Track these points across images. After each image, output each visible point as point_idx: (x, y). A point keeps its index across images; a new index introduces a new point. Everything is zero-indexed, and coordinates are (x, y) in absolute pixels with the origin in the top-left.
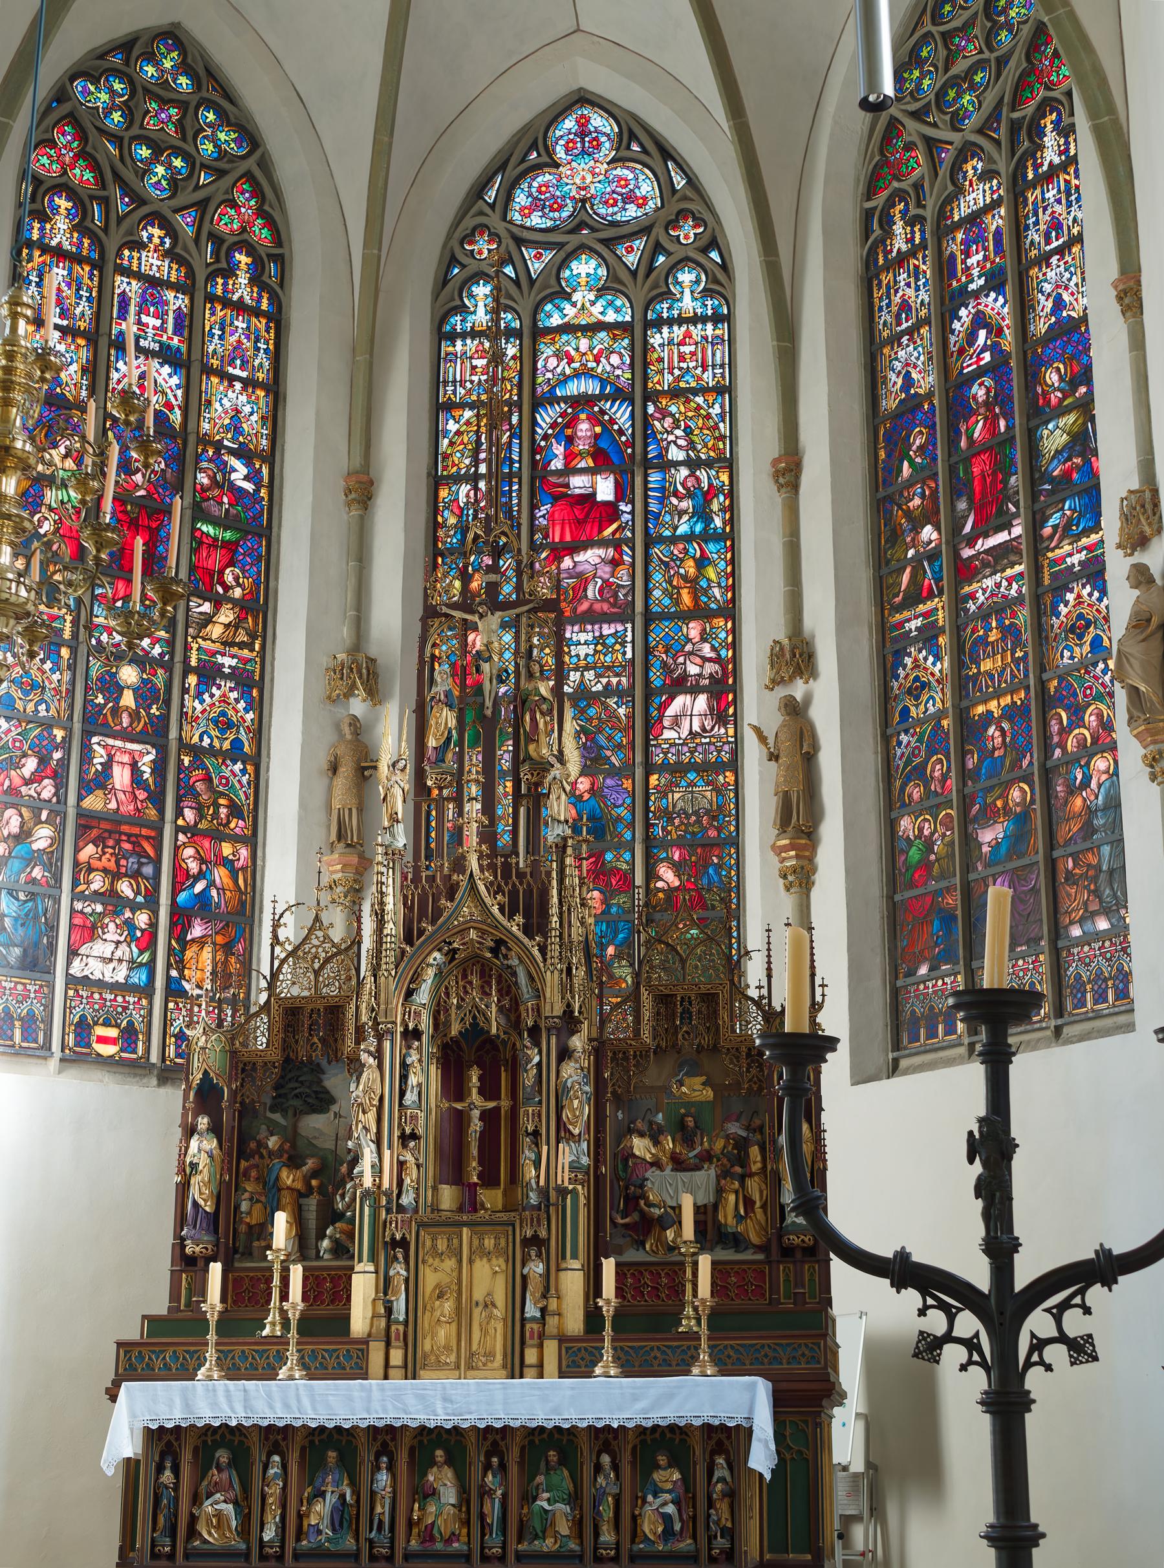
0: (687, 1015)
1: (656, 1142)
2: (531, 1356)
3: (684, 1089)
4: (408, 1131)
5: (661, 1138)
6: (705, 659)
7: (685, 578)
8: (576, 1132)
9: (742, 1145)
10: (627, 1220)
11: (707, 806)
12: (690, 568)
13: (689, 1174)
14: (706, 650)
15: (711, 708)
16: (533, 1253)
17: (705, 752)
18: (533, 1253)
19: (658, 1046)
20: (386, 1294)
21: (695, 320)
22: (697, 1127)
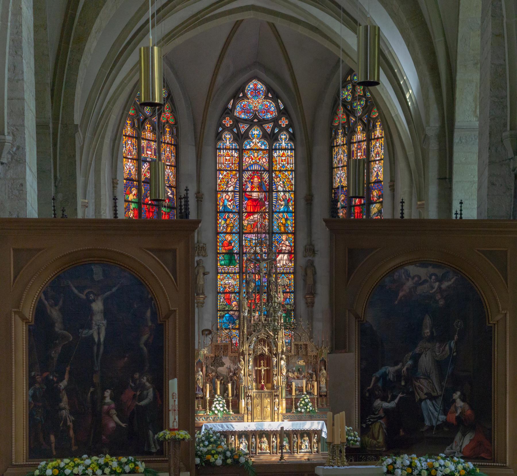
1: (294, 374)
2: (276, 417)
6: (287, 246)
7: (282, 223)
9: (311, 375)
12: (283, 221)
14: (287, 243)
15: (288, 258)
21: (285, 149)
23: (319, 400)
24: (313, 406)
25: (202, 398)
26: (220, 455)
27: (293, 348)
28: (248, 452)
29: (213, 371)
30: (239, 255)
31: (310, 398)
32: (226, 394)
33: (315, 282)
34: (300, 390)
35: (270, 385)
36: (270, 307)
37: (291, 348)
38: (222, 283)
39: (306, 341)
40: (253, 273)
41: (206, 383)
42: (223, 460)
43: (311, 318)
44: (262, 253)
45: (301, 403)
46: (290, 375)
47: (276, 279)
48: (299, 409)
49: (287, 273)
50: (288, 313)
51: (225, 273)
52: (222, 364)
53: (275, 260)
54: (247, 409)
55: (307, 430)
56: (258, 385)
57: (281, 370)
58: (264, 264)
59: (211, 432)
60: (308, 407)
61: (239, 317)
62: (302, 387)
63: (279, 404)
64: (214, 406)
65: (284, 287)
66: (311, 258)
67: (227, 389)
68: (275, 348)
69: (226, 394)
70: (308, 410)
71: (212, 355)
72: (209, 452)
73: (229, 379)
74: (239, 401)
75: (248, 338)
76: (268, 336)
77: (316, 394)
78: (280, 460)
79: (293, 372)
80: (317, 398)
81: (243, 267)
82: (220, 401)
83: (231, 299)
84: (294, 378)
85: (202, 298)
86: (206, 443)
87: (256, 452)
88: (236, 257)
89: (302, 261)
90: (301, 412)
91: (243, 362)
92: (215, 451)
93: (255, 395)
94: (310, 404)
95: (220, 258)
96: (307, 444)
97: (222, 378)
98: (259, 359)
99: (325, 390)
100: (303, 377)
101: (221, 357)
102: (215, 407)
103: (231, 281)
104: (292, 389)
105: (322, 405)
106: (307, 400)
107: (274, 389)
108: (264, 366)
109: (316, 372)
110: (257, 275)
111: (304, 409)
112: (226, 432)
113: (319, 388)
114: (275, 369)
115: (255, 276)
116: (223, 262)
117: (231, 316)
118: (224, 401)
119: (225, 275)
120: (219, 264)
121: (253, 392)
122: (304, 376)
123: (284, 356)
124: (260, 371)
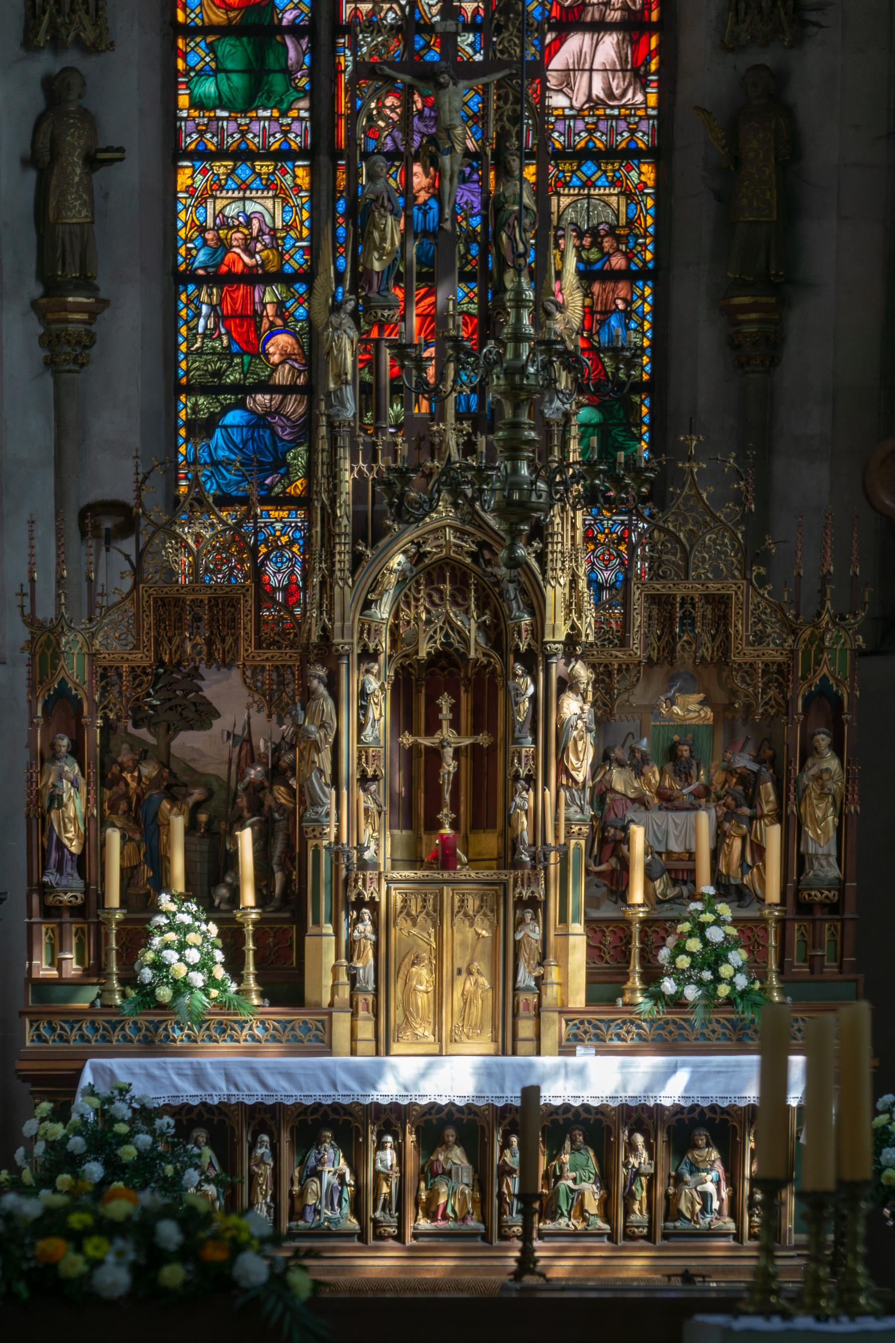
0: (688, 620)
1: (639, 774)
2: (526, 1028)
3: (676, 709)
4: (370, 772)
5: (646, 769)
8: (580, 778)
9: (749, 785)
10: (603, 867)
11: (611, 218)
13: (683, 814)
15: (623, 59)
16: (528, 916)
17: (612, 132)
18: (528, 916)
19: (649, 658)
20: (350, 958)
22: (692, 757)
23: (795, 932)
24: (755, 967)
25: (78, 911)
26: (119, 1243)
27: (638, 620)
28: (353, 1224)
29: (144, 756)
30: (314, 41)
31: (736, 922)
32: (224, 892)
33: (790, 208)
34: (674, 870)
35: (489, 842)
36: (489, 366)
37: (626, 618)
38: (208, 214)
39: (718, 575)
40: (393, 156)
41: (104, 823)
42: (135, 1270)
43: (757, 434)
44: (451, 26)
45: (680, 949)
46: (619, 780)
47: (542, 191)
48: (669, 986)
49: (611, 154)
50: (612, 399)
51: (221, 154)
52: (203, 715)
53: (539, 69)
54: (353, 979)
55: (713, 1108)
56: (417, 840)
57: (562, 750)
58: (463, 98)
59: (122, 1109)
60: (726, 971)
61: (306, 430)
62: (691, 856)
63: (544, 956)
64: (150, 956)
65: (597, 243)
66: (766, 57)
67: (232, 860)
68: (526, 620)
69: (224, 892)
70: (723, 990)
71: (143, 658)
72: (52, 1222)
73: (242, 801)
74: (302, 931)
75: (357, 560)
76: (482, 545)
77: (773, 894)
78: (518, 1275)
79: (638, 767)
80: (782, 922)
81: (333, 114)
82: (188, 929)
83: (256, 317)
84: (641, 801)
85: (79, 308)
86: (95, 1170)
87: (401, 1225)
88: (294, 51)
89: (710, 76)
90: (677, 1002)
91: (328, 705)
92: (88, 1219)
93: (397, 897)
94: (738, 957)
95: (193, 60)
96: (710, 1187)
97: (197, 794)
98: (418, 687)
99: (833, 872)
100: (696, 795)
101: (195, 674)
102: (159, 966)
103: (263, 208)
104: (625, 865)
105: (811, 961)
106: (715, 934)
107: (517, 865)
108: (455, 724)
109: (781, 765)
110: (417, 168)
111: (700, 983)
112: (223, 1109)
113: (796, 862)
114: (527, 746)
115: (409, 175)
116: (208, 87)
117: (260, 421)
118: (213, 929)
119: (221, 168)
120: (184, 101)
121: (389, 881)
122: (705, 792)
123: (582, 671)
124: (434, 755)
